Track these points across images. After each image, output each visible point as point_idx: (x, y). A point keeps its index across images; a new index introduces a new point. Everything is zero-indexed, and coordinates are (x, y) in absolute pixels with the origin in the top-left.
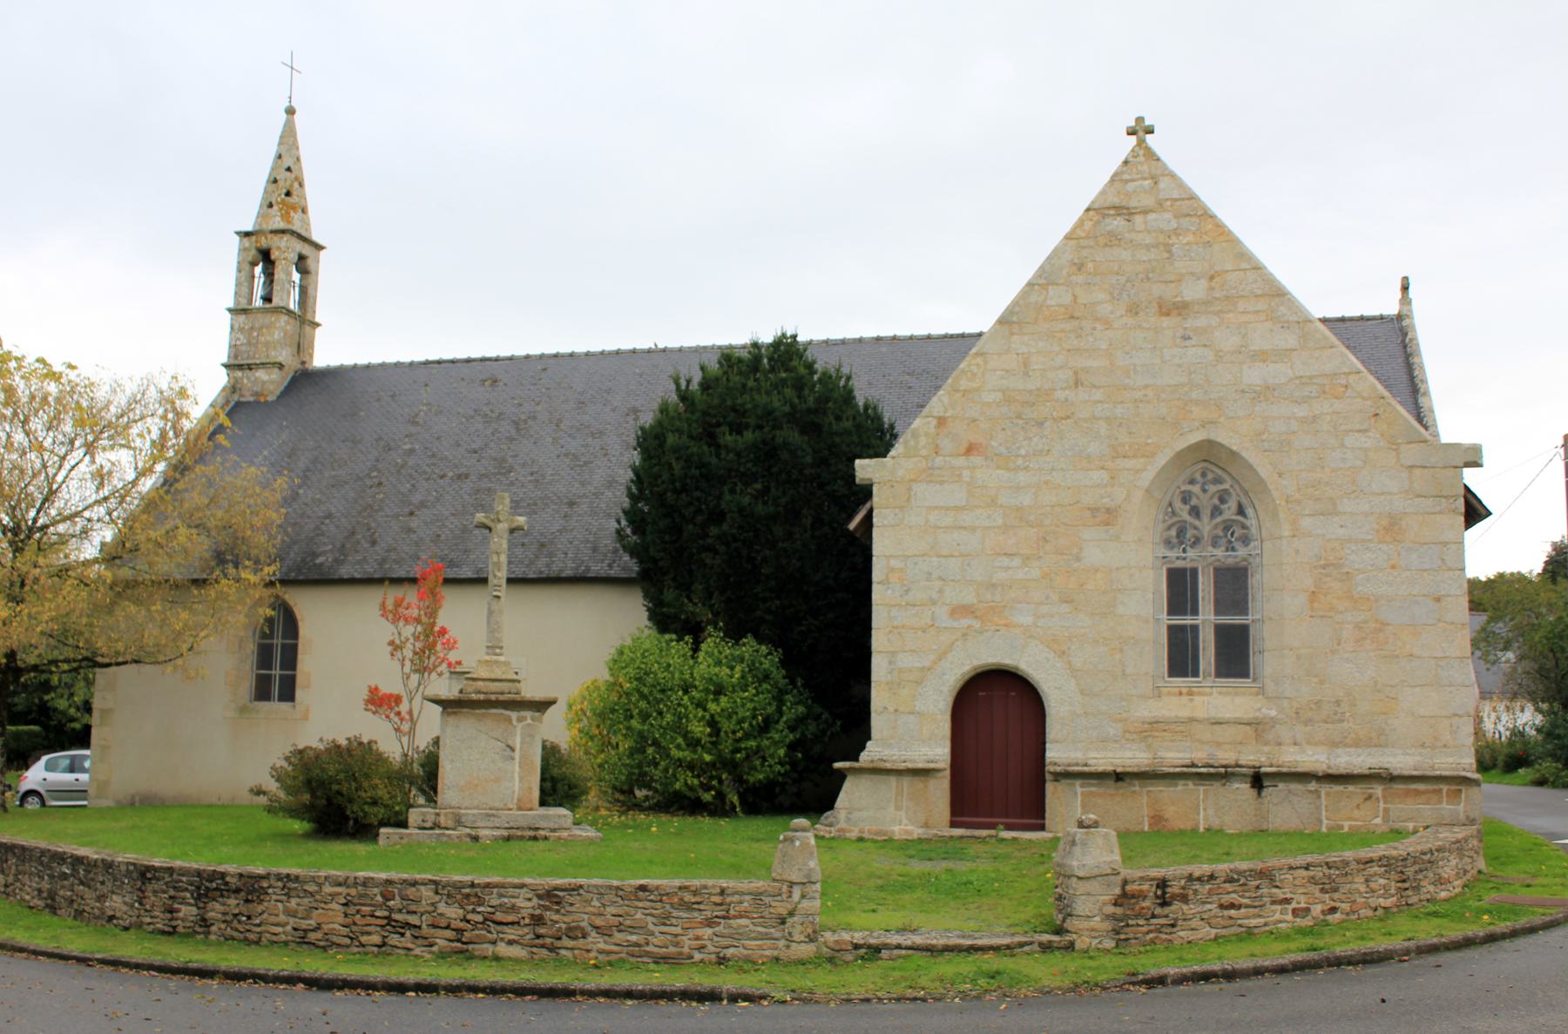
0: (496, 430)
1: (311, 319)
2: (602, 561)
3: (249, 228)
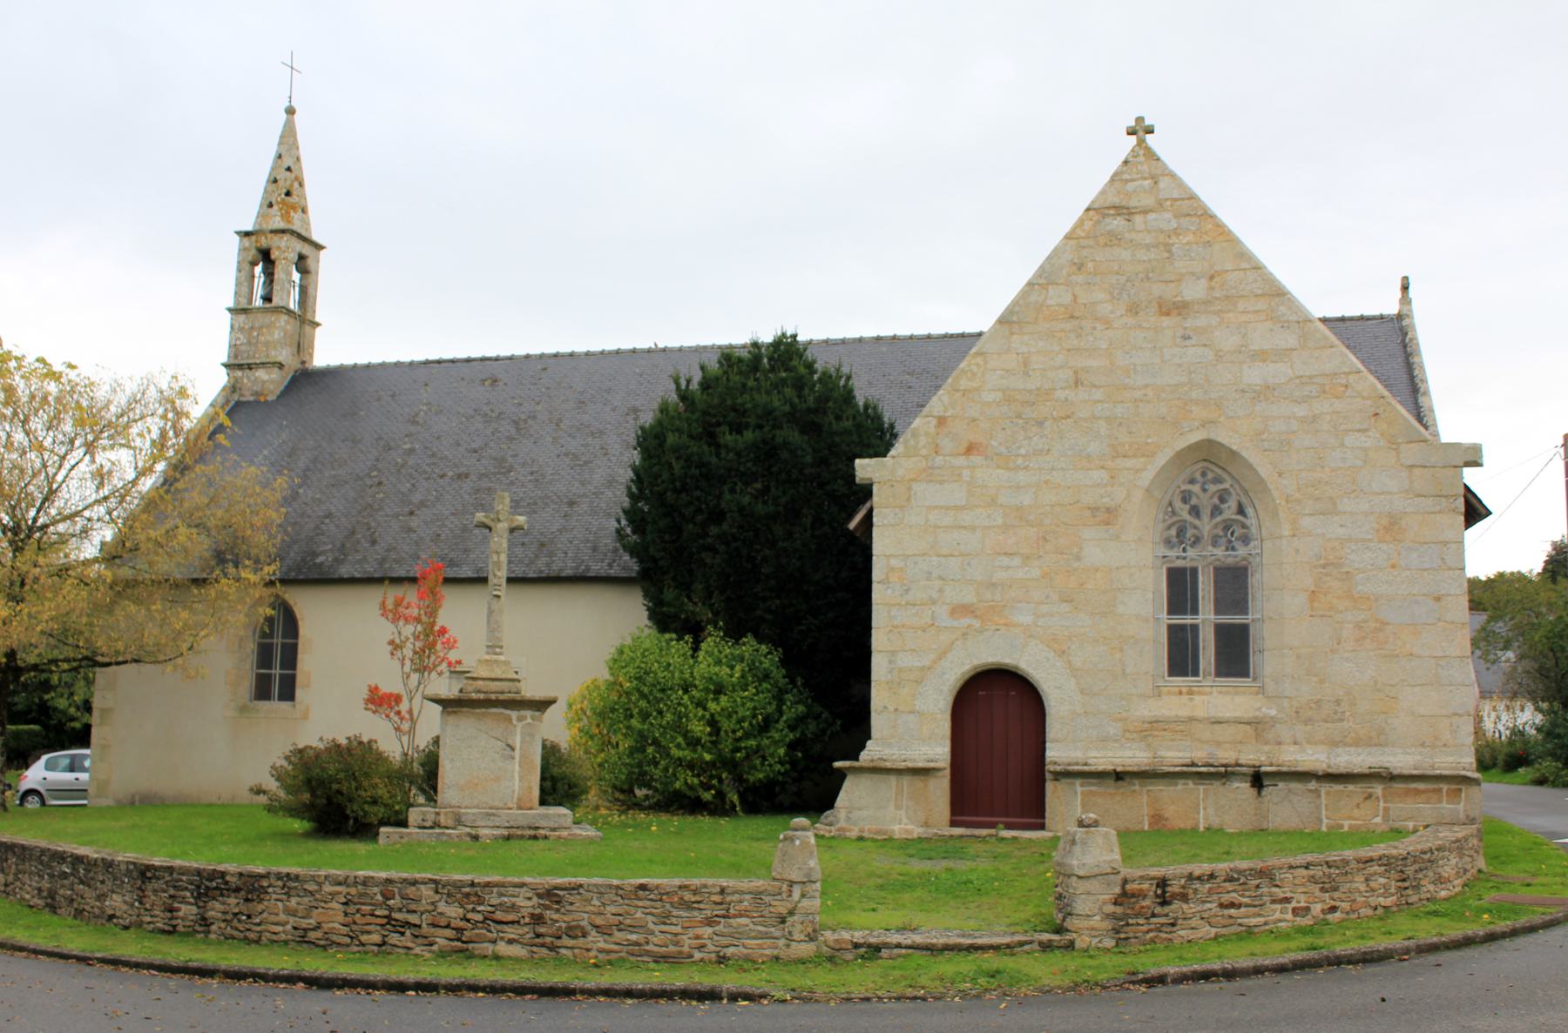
0: (496, 429)
1: (311, 319)
2: (602, 561)
3: (249, 228)
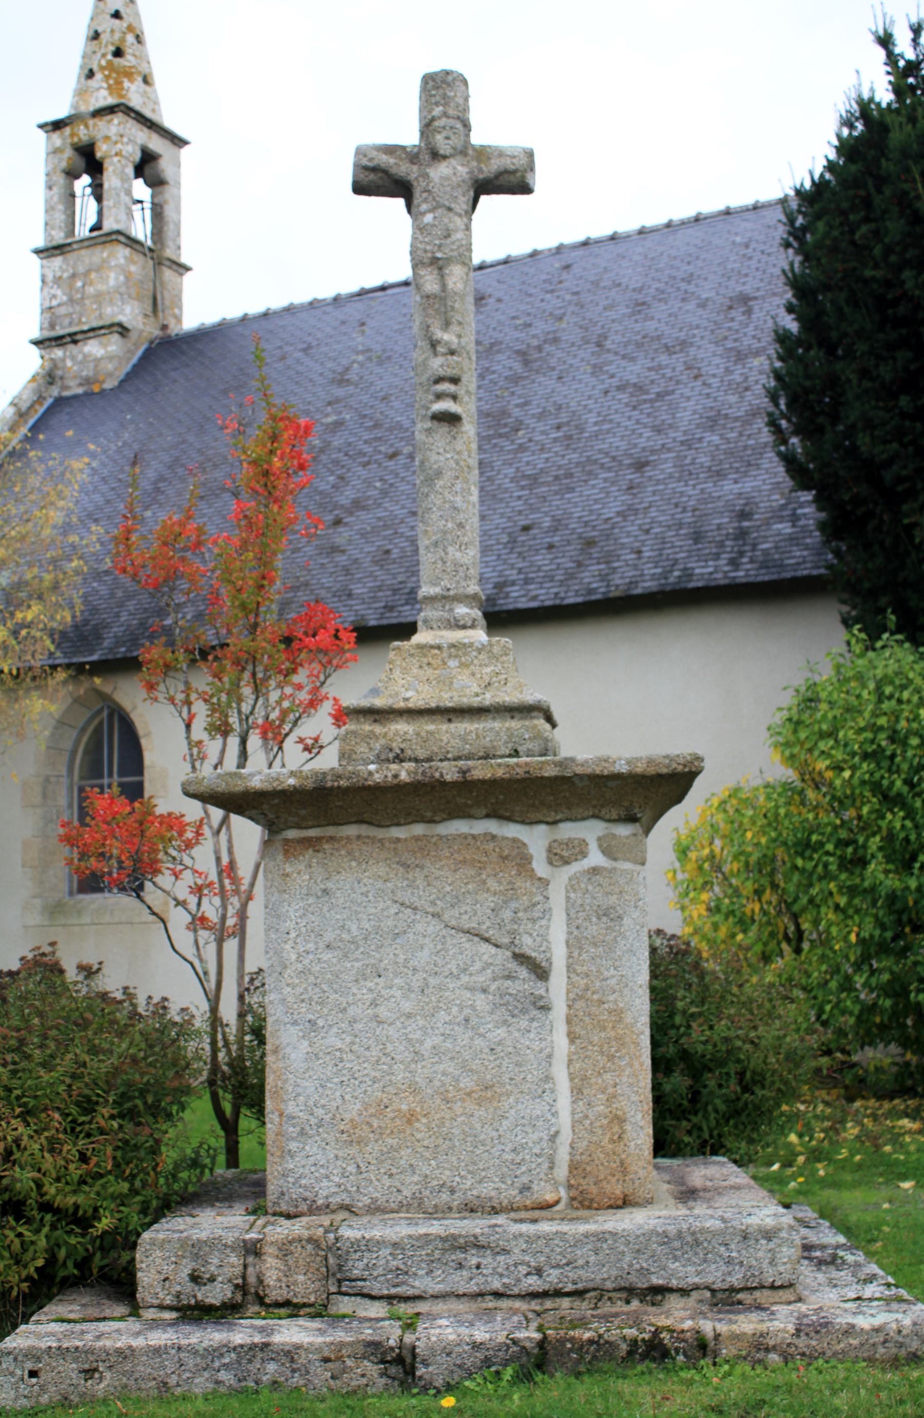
0: (487, 369)
1: (174, 257)
2: (717, 557)
3: (61, 113)
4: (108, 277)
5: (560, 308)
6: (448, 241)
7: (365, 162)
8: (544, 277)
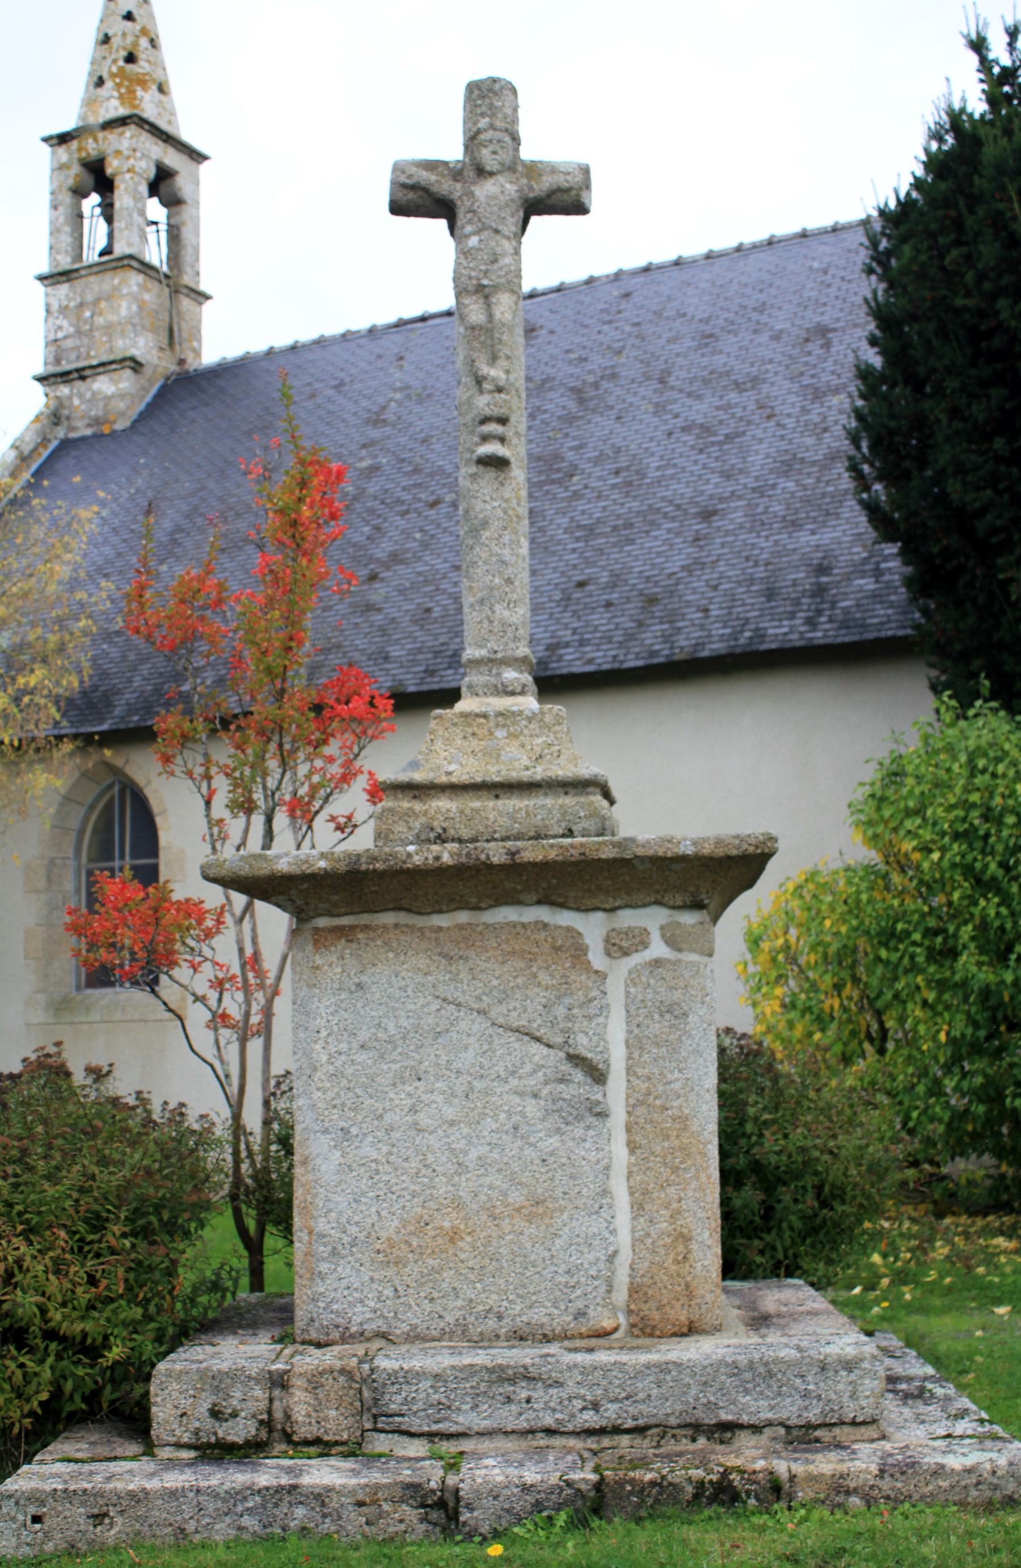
0: (539, 408)
1: (192, 285)
2: (792, 615)
3: (68, 125)
4: (119, 306)
5: (619, 341)
6: (495, 266)
7: (403, 179)
8: (602, 306)
